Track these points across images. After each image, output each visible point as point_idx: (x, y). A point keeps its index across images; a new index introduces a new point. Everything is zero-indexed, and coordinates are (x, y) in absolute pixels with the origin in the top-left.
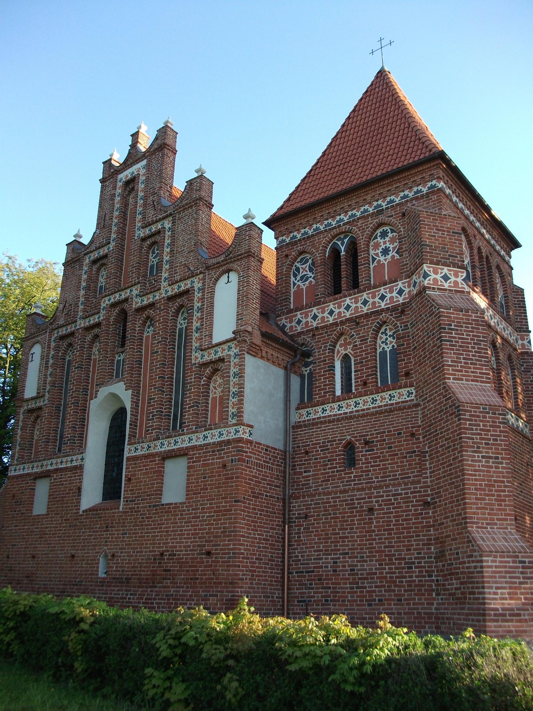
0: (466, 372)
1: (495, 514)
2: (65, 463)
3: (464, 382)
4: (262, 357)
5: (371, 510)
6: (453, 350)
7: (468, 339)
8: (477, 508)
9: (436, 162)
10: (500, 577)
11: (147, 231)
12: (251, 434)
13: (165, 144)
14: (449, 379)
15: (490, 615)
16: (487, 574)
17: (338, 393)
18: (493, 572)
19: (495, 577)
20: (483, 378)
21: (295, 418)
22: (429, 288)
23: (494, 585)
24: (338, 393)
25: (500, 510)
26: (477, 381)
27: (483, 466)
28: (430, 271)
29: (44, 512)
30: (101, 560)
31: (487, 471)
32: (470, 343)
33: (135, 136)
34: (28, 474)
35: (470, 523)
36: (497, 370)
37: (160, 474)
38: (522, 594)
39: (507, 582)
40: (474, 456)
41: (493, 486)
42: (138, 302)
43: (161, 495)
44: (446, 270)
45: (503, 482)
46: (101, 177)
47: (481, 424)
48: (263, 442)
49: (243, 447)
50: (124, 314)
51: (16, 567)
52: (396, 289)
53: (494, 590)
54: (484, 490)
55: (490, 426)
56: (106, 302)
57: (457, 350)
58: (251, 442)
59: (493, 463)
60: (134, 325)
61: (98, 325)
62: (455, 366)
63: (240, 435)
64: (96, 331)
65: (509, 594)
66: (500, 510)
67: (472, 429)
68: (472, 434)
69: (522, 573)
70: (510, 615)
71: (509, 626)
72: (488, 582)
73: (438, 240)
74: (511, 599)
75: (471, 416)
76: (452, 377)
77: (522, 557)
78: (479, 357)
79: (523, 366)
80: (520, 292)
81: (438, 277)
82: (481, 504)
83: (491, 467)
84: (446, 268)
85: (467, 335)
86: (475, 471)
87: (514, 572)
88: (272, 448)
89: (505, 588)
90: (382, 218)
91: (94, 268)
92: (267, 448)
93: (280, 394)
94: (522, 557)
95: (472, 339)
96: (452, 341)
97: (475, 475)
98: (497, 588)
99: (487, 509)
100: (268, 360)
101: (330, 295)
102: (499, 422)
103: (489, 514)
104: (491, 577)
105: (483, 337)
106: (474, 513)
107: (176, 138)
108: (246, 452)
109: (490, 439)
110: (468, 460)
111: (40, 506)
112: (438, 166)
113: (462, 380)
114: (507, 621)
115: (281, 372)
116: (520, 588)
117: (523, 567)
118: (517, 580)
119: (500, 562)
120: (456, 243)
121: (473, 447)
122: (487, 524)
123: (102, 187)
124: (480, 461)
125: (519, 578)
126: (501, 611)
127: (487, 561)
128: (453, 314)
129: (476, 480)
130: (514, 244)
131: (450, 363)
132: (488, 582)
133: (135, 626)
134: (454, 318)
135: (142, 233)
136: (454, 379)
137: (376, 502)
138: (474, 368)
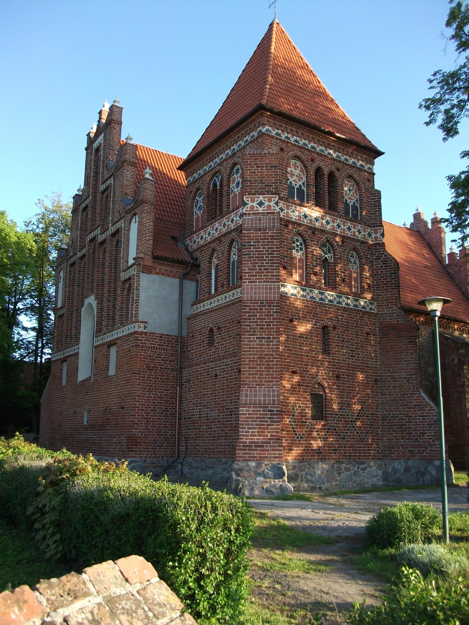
0: (259, 276)
1: (264, 378)
2: (69, 352)
3: (257, 284)
4: (157, 273)
5: (216, 376)
6: (250, 261)
7: (263, 251)
8: (249, 374)
9: (260, 112)
10: (251, 421)
12: (145, 328)
13: (111, 120)
14: (245, 282)
15: (240, 446)
17: (213, 292)
18: (246, 418)
19: (248, 421)
20: (273, 279)
21: (188, 311)
22: (246, 214)
23: (247, 427)
24: (213, 292)
25: (268, 375)
26: (268, 282)
27: (256, 344)
28: (248, 201)
30: (86, 414)
31: (260, 348)
32: (265, 254)
33: (100, 113)
34: (58, 360)
35: (243, 384)
36: (334, 263)
38: (268, 432)
39: (257, 425)
40: (251, 338)
41: (264, 358)
43: (108, 370)
44: (261, 198)
45: (273, 355)
47: (258, 314)
48: (157, 332)
49: (138, 337)
52: (264, 207)
53: (246, 430)
54: (257, 361)
55: (265, 316)
57: (253, 260)
58: (146, 333)
59: (265, 342)
62: (251, 273)
63: (136, 329)
65: (258, 432)
66: (268, 375)
67: (250, 319)
68: (250, 322)
69: (270, 418)
70: (255, 446)
71: (254, 454)
72: (243, 425)
73: (258, 175)
74: (259, 436)
75: (249, 309)
76: (247, 281)
77: (271, 407)
78: (271, 263)
79: (375, 254)
80: (378, 193)
81: (255, 204)
82: (253, 371)
83: (264, 345)
84: (261, 196)
85: (263, 248)
86: (250, 348)
87: (264, 418)
88: (166, 335)
89: (255, 428)
92: (161, 336)
93: (176, 296)
94: (271, 407)
95: (266, 251)
96: (250, 254)
97: (250, 351)
98: (249, 428)
99: (257, 374)
100: (163, 274)
101: (208, 220)
102: (273, 312)
103: (259, 378)
104: (245, 421)
105: (276, 248)
106: (247, 378)
107: (121, 112)
108: (142, 340)
109: (264, 325)
110: (245, 341)
112: (262, 115)
113: (256, 282)
114: (253, 450)
115: (176, 281)
116: (268, 429)
117: (271, 414)
118: (266, 423)
119: (252, 411)
120: (272, 175)
121: (250, 332)
122: (257, 385)
123: (87, 154)
124: (255, 341)
125: (267, 422)
126: (248, 444)
127: (243, 411)
128: (253, 233)
129: (250, 355)
130: (377, 153)
131: (247, 271)
132: (243, 425)
134: (254, 236)
136: (249, 282)
137: (219, 370)
138: (266, 272)
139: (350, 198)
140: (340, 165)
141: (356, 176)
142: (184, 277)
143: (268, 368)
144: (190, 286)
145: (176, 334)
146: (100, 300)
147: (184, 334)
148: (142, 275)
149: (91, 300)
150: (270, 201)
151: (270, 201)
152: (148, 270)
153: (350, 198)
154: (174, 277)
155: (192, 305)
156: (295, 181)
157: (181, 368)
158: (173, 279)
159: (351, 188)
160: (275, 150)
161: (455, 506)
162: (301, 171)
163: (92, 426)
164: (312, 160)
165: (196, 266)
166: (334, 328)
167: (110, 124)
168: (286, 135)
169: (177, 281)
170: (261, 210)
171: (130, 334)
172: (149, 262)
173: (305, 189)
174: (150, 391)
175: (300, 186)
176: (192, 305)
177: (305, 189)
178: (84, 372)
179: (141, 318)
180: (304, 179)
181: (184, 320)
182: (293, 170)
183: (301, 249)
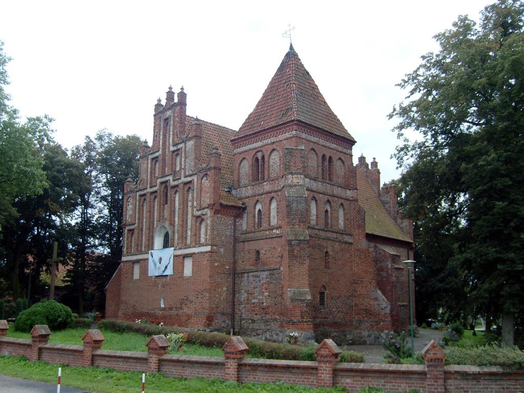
11: (176, 148)
16: (441, 373)
29: (138, 278)
37: (183, 264)
42: (173, 183)
46: (154, 113)
50: (166, 187)
51: (71, 360)
56: (159, 181)
60: (170, 192)
61: (156, 192)
64: (156, 194)
90: (274, 146)
91: (154, 162)
111: (136, 275)
133: (120, 138)
135: (172, 149)
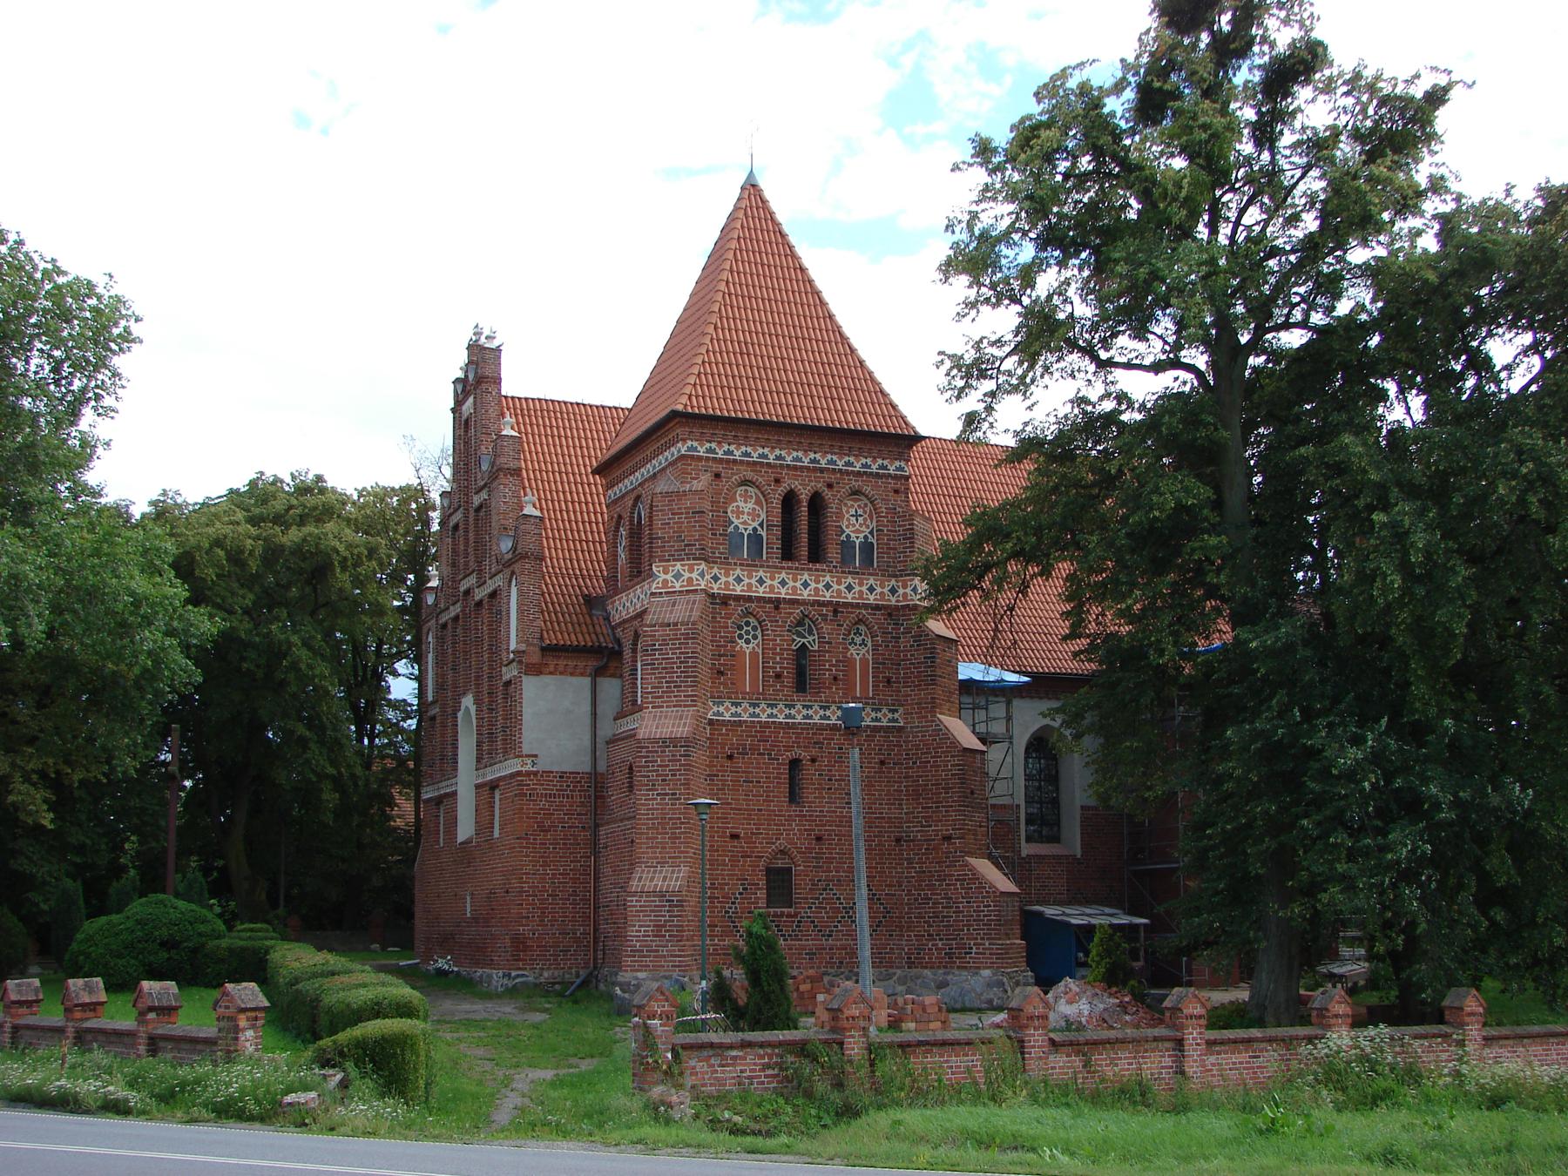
12: (534, 764)
21: (607, 729)
44: (678, 566)
58: (535, 774)
92: (562, 775)
93: (586, 707)
139: (857, 531)
140: (833, 478)
141: (867, 489)
142: (598, 673)
143: (674, 838)
144: (610, 688)
145: (588, 768)
146: (478, 702)
147: (602, 767)
148: (524, 678)
149: (468, 701)
150: (691, 570)
151: (691, 570)
152: (535, 670)
153: (857, 531)
154: (582, 674)
155: (615, 719)
156: (744, 523)
157: (597, 826)
158: (581, 679)
159: (860, 512)
160: (706, 478)
161: (1494, 1032)
162: (758, 502)
163: (475, 919)
164: (777, 481)
165: (617, 654)
166: (813, 760)
167: (480, 372)
168: (726, 447)
169: (586, 681)
170: (678, 586)
171: (512, 776)
172: (535, 657)
173: (764, 534)
174: (545, 864)
175: (755, 529)
176: (615, 719)
177: (764, 534)
178: (465, 829)
179: (526, 750)
180: (763, 516)
181: (600, 745)
182: (741, 504)
183: (755, 637)
